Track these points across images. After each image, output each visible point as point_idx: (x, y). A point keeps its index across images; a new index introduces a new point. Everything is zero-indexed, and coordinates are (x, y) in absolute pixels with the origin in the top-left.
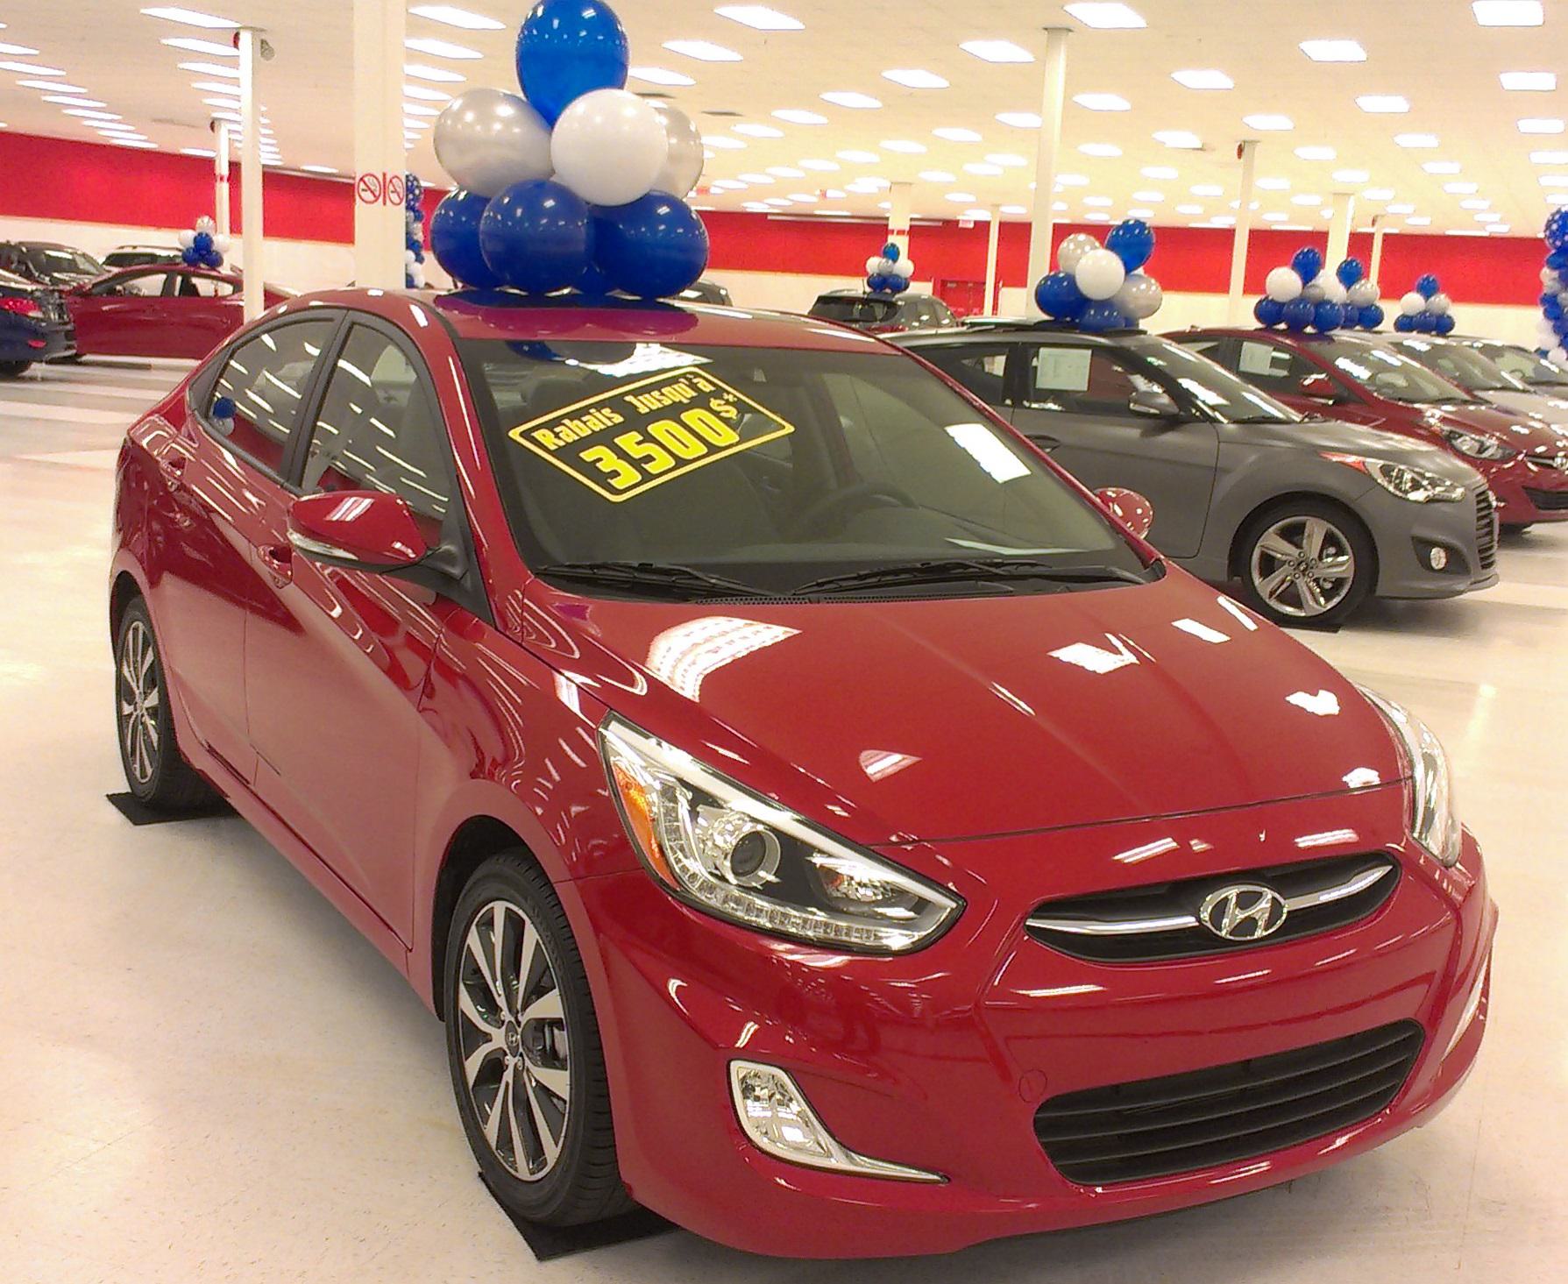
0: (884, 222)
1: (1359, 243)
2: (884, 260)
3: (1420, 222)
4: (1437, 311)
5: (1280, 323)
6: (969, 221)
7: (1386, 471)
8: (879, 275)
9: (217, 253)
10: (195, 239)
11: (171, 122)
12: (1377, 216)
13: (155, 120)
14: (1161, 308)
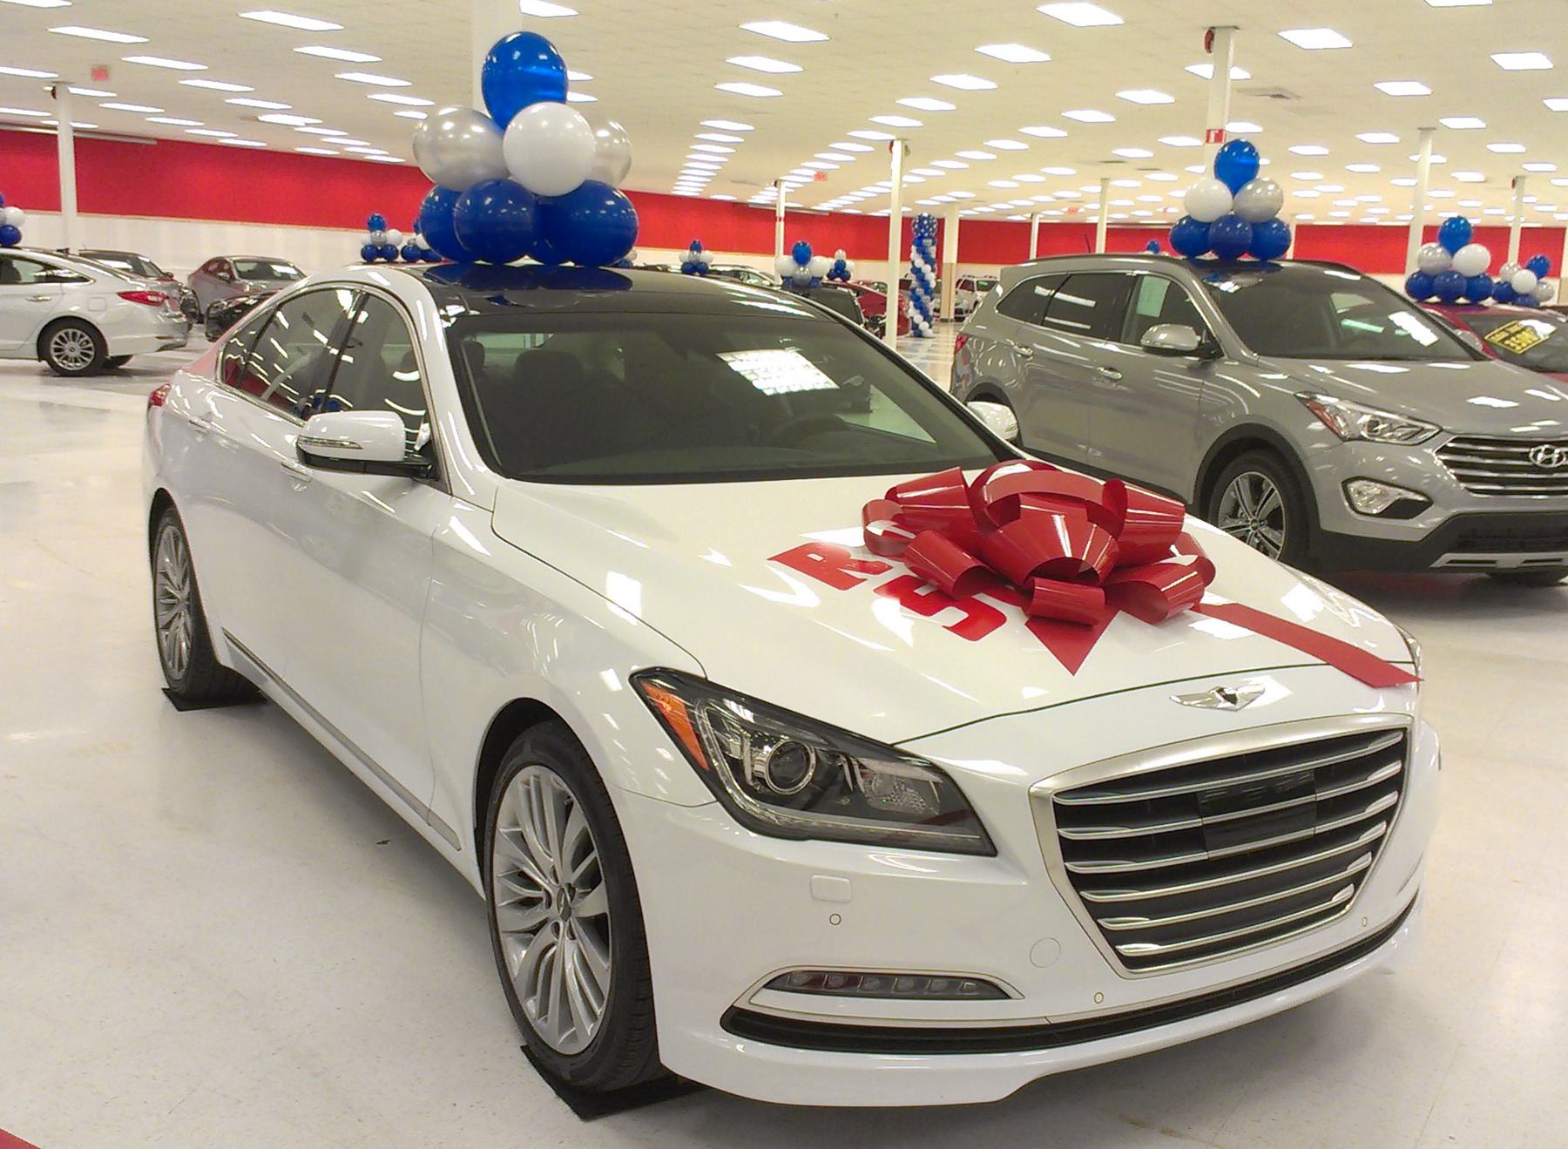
5: (1433, 295)
9: (847, 272)
10: (836, 264)
11: (744, 182)
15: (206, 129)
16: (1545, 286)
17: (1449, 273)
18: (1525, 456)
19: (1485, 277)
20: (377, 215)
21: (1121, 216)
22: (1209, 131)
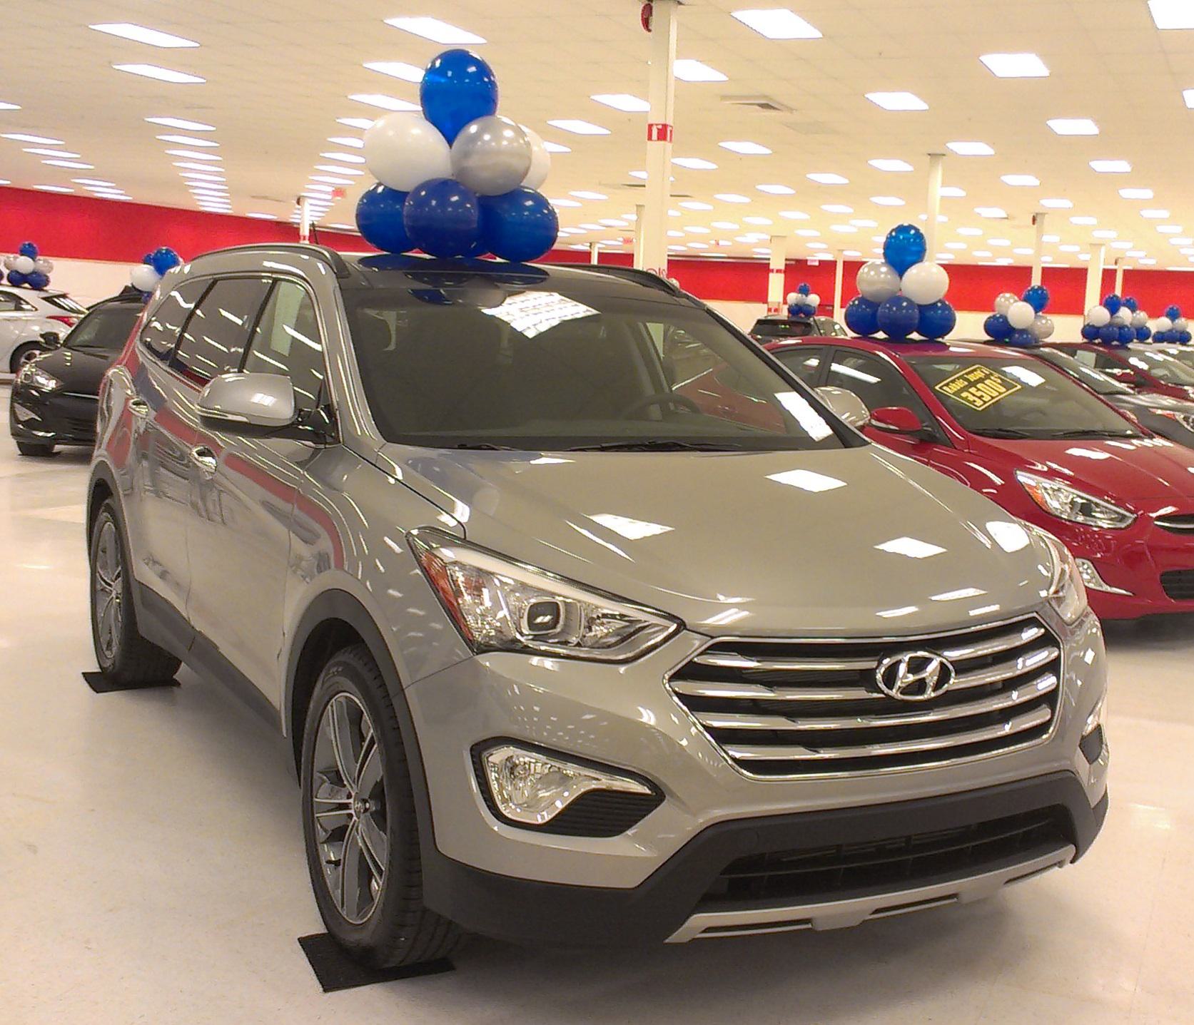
0: (767, 262)
1: (1109, 276)
2: (800, 295)
3: (1148, 262)
4: (1180, 329)
6: (815, 261)
7: (1186, 419)
8: (796, 305)
11: (265, 198)
12: (1037, 214)
13: (253, 197)
14: (1054, 333)
15: (118, 189)
16: (1044, 321)
17: (897, 299)
18: (865, 678)
19: (945, 307)
20: (27, 243)
21: (680, 249)
22: (650, 126)
